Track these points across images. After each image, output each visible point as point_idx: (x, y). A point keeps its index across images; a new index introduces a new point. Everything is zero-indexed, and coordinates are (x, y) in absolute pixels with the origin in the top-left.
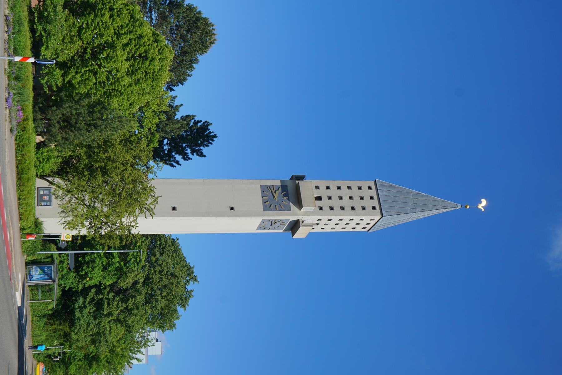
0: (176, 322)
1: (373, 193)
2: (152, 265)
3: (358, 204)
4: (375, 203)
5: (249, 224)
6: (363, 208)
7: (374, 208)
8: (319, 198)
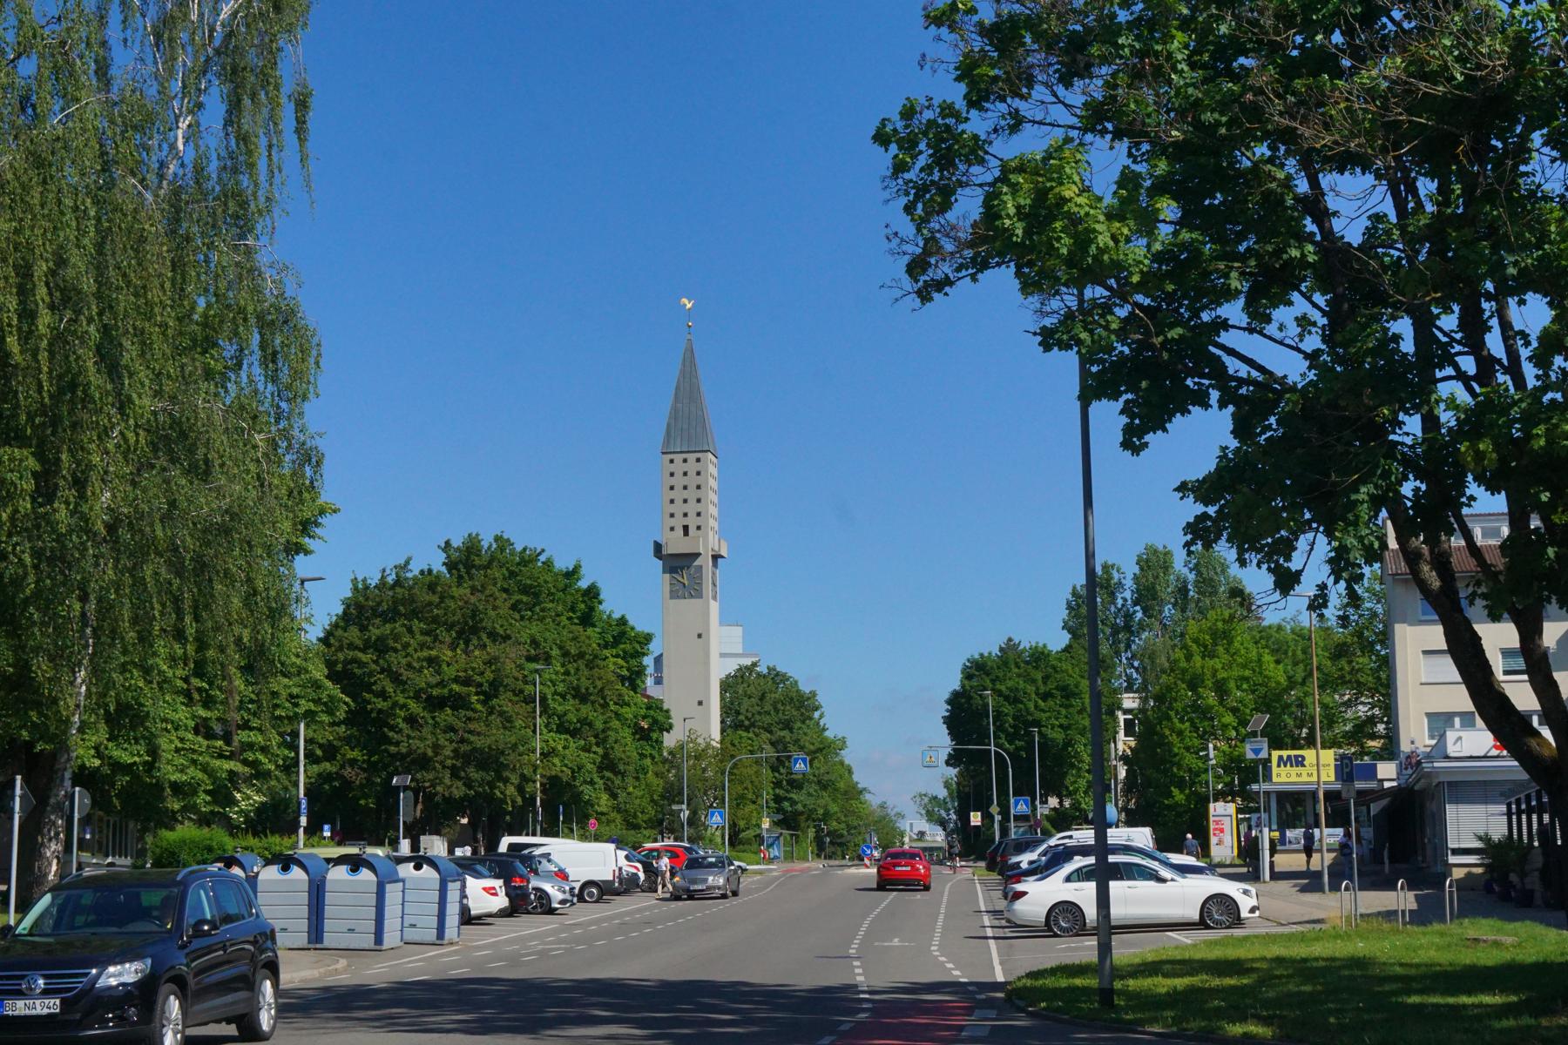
0: (487, 540)
1: (678, 458)
2: (753, 725)
3: (692, 480)
4: (692, 457)
5: (714, 607)
8: (686, 528)
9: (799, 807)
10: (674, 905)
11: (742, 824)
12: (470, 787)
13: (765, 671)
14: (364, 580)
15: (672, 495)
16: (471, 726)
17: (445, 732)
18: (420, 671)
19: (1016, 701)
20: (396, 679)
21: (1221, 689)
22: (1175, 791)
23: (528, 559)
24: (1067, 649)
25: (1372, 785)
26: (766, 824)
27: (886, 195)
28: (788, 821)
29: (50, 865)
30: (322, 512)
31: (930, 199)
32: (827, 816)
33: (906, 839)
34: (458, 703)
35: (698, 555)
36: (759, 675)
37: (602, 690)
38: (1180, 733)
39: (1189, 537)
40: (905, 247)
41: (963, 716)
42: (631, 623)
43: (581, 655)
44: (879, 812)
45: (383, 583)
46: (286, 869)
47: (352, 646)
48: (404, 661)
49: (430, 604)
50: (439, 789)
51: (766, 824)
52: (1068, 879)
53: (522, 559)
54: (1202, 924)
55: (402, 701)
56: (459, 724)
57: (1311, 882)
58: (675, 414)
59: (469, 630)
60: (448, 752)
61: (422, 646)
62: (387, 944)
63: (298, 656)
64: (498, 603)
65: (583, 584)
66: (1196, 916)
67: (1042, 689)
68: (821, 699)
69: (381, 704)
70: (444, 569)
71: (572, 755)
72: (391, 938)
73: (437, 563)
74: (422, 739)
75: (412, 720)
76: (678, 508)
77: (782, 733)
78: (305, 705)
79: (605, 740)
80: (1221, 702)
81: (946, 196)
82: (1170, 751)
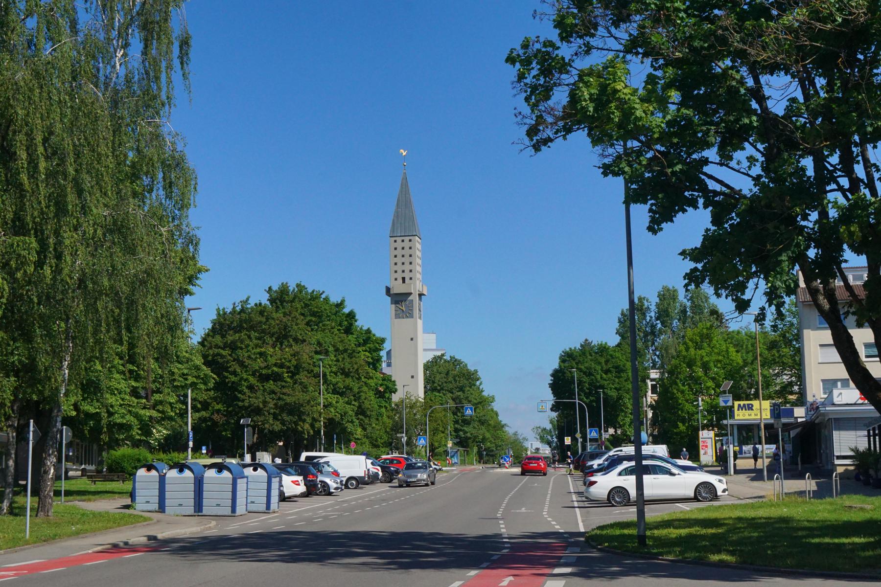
0: (292, 287)
1: (399, 239)
4: (407, 239)
5: (420, 323)
6: (410, 248)
7: (410, 241)
8: (404, 279)
9: (469, 435)
11: (436, 444)
12: (284, 424)
13: (449, 359)
16: (284, 391)
18: (255, 360)
19: (590, 374)
20: (242, 364)
21: (706, 367)
22: (680, 425)
23: (315, 297)
24: (619, 345)
25: (792, 420)
26: (450, 444)
27: (515, 92)
28: (463, 443)
30: (200, 271)
31: (539, 94)
32: (484, 440)
34: (277, 377)
36: (445, 361)
37: (357, 370)
38: (683, 392)
39: (687, 281)
41: (560, 383)
42: (373, 332)
43: (346, 350)
45: (234, 311)
46: (181, 471)
48: (246, 355)
49: (260, 322)
52: (620, 474)
53: (312, 296)
54: (696, 499)
55: (245, 377)
56: (277, 390)
57: (757, 475)
58: (397, 215)
59: (282, 337)
60: (271, 405)
61: (257, 346)
63: (187, 352)
65: (346, 311)
66: (692, 495)
67: (605, 367)
68: (551, 372)
69: (233, 379)
70: (268, 303)
72: (240, 509)
73: (264, 299)
74: (256, 398)
77: (459, 393)
78: (191, 379)
79: (359, 398)
80: (706, 374)
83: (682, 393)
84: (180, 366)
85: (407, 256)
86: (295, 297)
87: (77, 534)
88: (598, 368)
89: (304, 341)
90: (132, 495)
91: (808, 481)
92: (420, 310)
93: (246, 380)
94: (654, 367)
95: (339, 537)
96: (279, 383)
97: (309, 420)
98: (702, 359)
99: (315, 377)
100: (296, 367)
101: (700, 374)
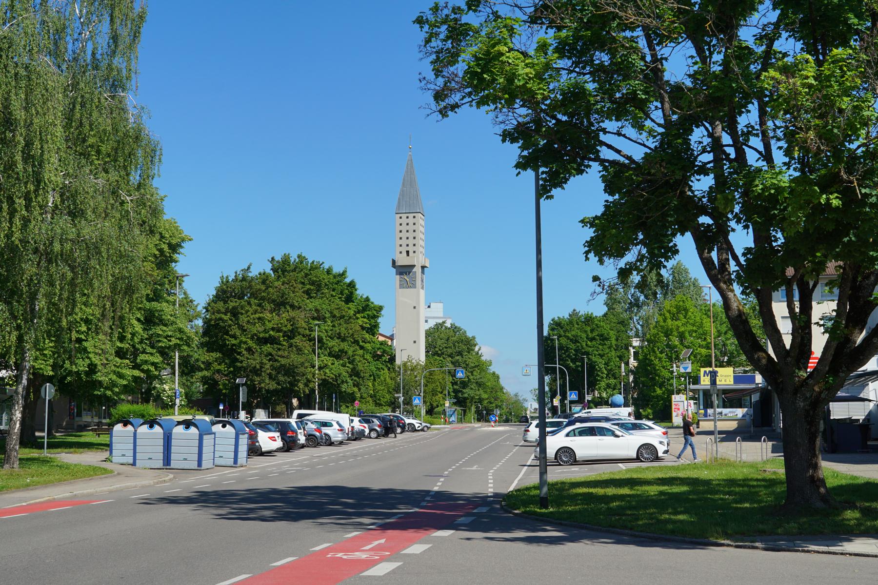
0: (293, 258)
1: (404, 216)
3: (411, 227)
5: (422, 293)
8: (408, 252)
9: (466, 395)
10: (355, 445)
11: (435, 404)
12: (278, 384)
13: (449, 326)
14: (227, 277)
15: (401, 235)
16: (280, 353)
17: (266, 356)
18: (254, 324)
19: (577, 341)
20: (241, 328)
21: (682, 337)
22: (658, 389)
23: (315, 267)
24: (605, 315)
25: (753, 386)
26: (447, 404)
27: (421, 55)
28: (461, 402)
29: (15, 424)
30: (183, 240)
31: (443, 61)
32: (481, 400)
33: (528, 412)
34: (272, 341)
35: (414, 266)
36: (446, 328)
37: (352, 335)
38: (660, 359)
39: (587, 249)
40: (429, 86)
41: (547, 351)
42: (372, 300)
43: (342, 317)
44: (515, 399)
45: (236, 280)
46: (151, 427)
47: (219, 312)
48: (246, 319)
49: (260, 290)
50: (263, 385)
51: (447, 404)
52: (567, 435)
53: (311, 267)
54: (638, 459)
55: (244, 340)
56: (274, 353)
57: (729, 436)
58: (403, 194)
59: (280, 304)
60: (268, 366)
61: (256, 312)
62: (204, 466)
63: (171, 315)
64: (296, 290)
65: (348, 280)
66: (635, 456)
67: (590, 335)
68: (477, 340)
69: (234, 341)
70: (271, 272)
71: (336, 368)
72: (206, 463)
73: (268, 268)
74: (254, 360)
75: (249, 350)
76: (404, 242)
77: (457, 358)
78: (174, 341)
79: (353, 361)
80: (682, 343)
81: (453, 57)
82: (654, 368)
83: (659, 361)
84: (165, 328)
85: (411, 231)
86: (296, 267)
87: (27, 487)
88: (584, 336)
89: (300, 308)
90: (109, 446)
91: (764, 444)
92: (422, 281)
93: (245, 343)
94: (637, 336)
95: (291, 492)
96: (275, 346)
97: (303, 380)
98: (677, 329)
99: (310, 340)
100: (292, 331)
101: (677, 343)
